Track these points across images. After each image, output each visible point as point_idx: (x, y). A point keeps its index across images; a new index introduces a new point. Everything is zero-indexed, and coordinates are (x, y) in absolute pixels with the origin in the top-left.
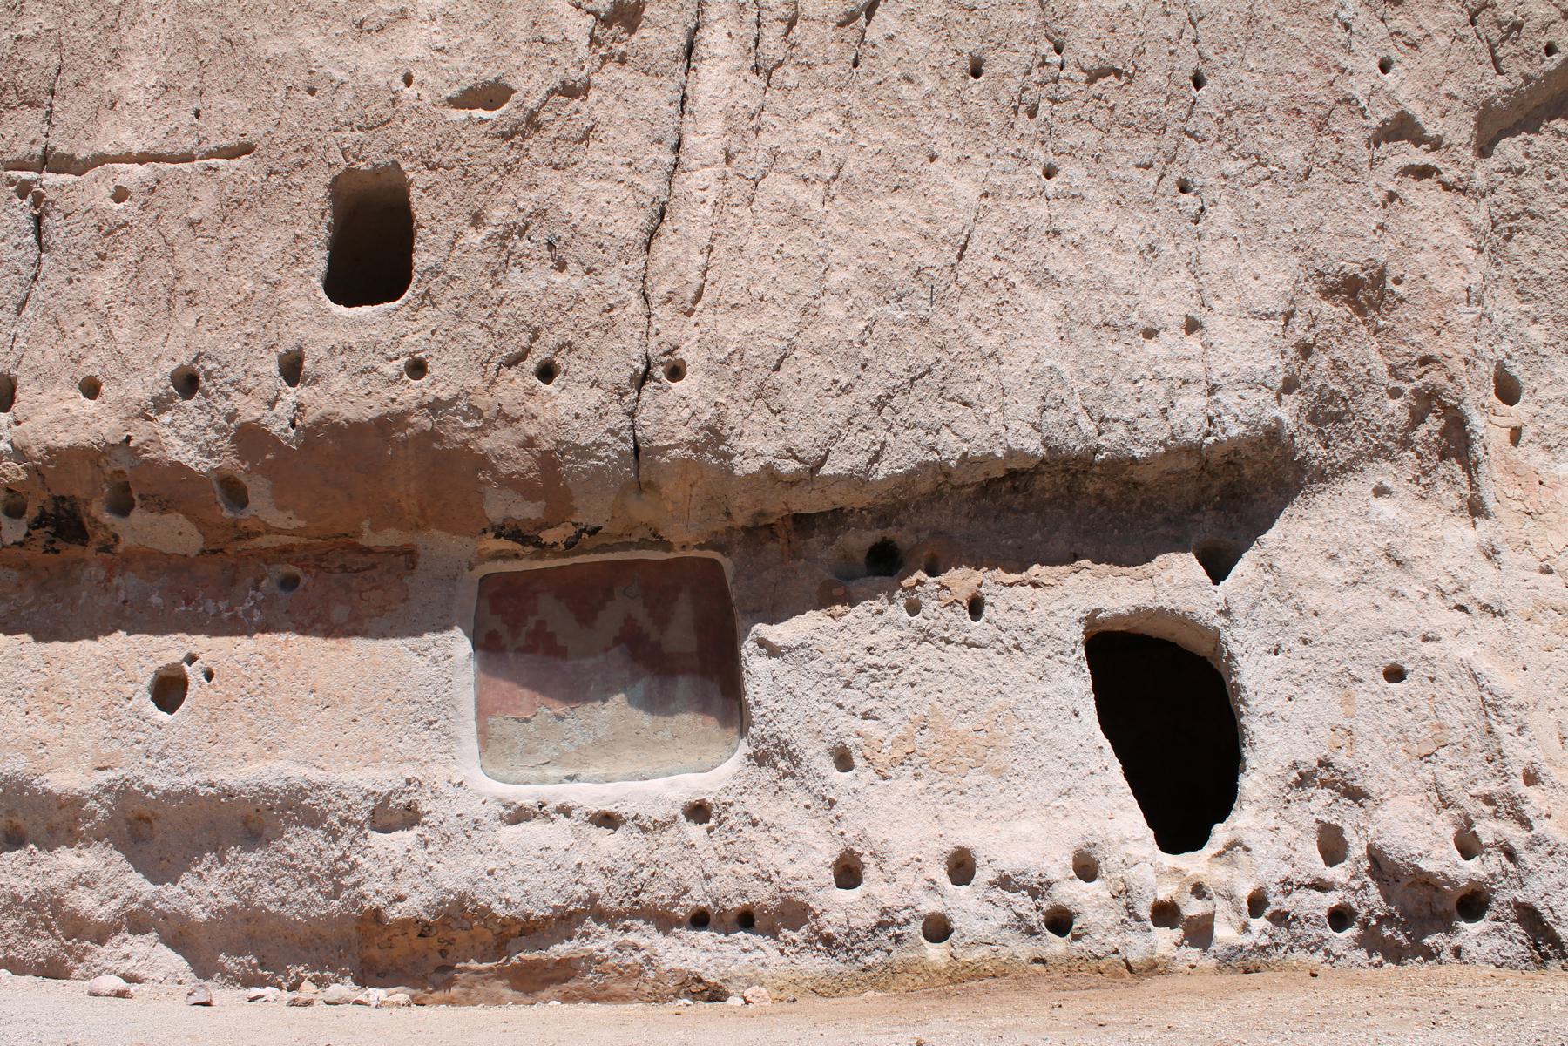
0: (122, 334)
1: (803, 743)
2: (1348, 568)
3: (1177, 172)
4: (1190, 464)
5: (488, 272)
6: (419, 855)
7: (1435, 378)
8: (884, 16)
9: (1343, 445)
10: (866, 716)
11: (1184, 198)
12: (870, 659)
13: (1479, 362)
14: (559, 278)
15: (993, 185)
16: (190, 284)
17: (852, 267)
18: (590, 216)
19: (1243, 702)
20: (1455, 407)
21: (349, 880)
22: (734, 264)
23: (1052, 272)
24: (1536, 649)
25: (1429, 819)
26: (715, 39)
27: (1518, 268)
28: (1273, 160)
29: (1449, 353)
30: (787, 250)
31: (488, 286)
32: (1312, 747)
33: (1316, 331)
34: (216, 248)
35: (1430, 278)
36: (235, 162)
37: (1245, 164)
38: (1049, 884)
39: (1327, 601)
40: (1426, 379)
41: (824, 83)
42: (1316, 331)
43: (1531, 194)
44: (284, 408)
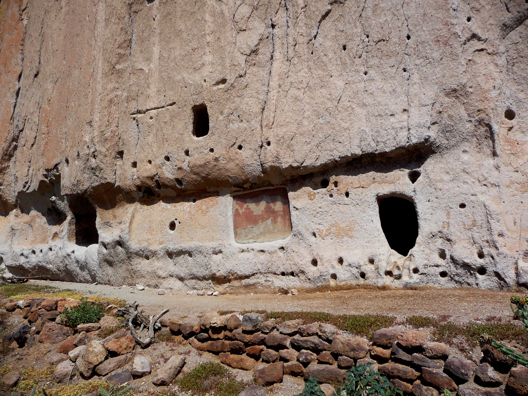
0: (154, 149)
1: (303, 231)
2: (451, 176)
3: (403, 66)
4: (404, 151)
5: (225, 126)
6: (222, 261)
7: (483, 115)
8: (319, 38)
9: (453, 139)
10: (319, 224)
11: (405, 73)
12: (320, 210)
13: (498, 108)
14: (241, 124)
15: (348, 81)
16: (166, 136)
17: (310, 110)
18: (247, 108)
19: (418, 216)
20: (489, 124)
21: (209, 267)
22: (281, 114)
23: (365, 103)
24: (509, 196)
25: (469, 247)
26: (277, 55)
27: (516, 75)
28: (430, 57)
29: (486, 107)
30: (294, 109)
31: (225, 129)
32: (436, 228)
33: (443, 107)
34: (170, 128)
35: (481, 85)
36: (172, 107)
37: (422, 60)
38: (360, 266)
39: (444, 186)
40: (480, 116)
41: (304, 61)
42: (443, 107)
43: (521, 50)
44: (186, 163)
